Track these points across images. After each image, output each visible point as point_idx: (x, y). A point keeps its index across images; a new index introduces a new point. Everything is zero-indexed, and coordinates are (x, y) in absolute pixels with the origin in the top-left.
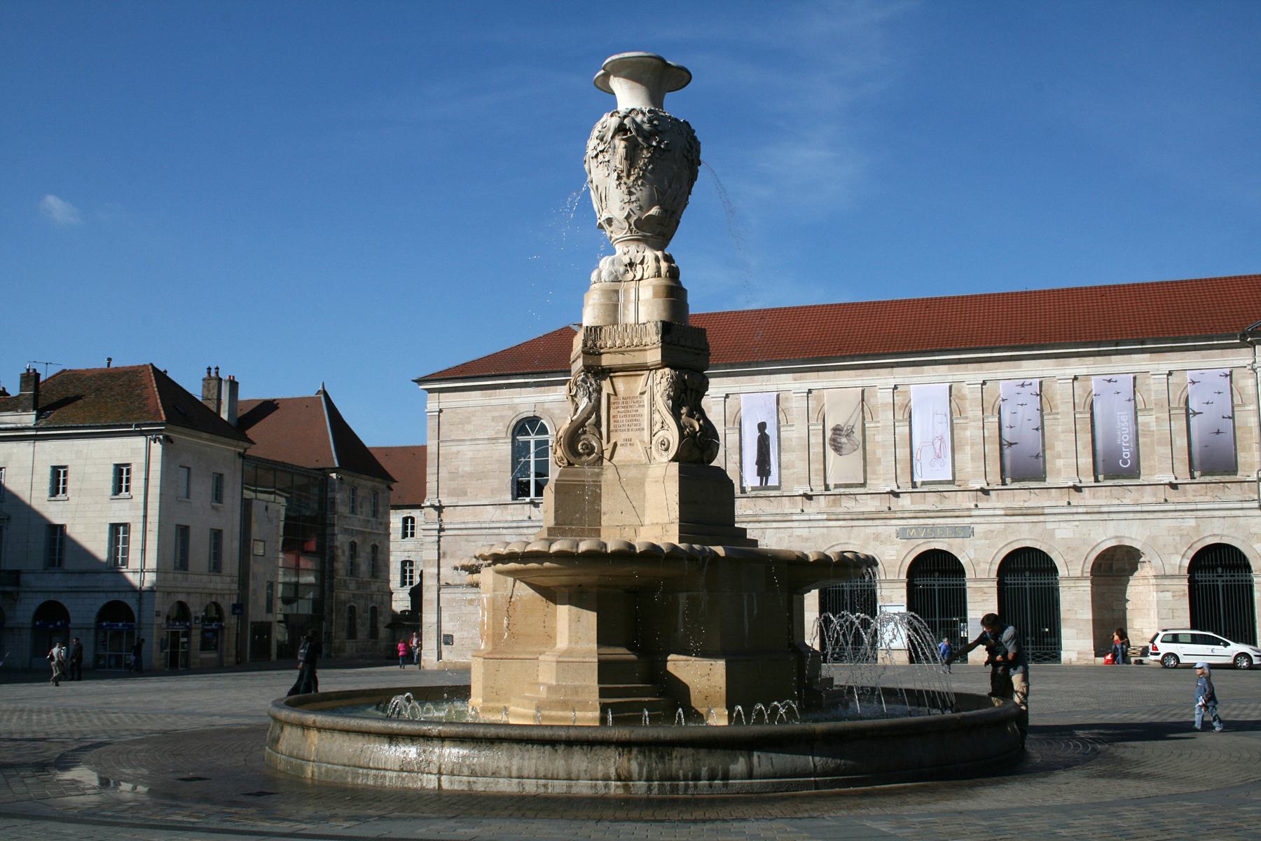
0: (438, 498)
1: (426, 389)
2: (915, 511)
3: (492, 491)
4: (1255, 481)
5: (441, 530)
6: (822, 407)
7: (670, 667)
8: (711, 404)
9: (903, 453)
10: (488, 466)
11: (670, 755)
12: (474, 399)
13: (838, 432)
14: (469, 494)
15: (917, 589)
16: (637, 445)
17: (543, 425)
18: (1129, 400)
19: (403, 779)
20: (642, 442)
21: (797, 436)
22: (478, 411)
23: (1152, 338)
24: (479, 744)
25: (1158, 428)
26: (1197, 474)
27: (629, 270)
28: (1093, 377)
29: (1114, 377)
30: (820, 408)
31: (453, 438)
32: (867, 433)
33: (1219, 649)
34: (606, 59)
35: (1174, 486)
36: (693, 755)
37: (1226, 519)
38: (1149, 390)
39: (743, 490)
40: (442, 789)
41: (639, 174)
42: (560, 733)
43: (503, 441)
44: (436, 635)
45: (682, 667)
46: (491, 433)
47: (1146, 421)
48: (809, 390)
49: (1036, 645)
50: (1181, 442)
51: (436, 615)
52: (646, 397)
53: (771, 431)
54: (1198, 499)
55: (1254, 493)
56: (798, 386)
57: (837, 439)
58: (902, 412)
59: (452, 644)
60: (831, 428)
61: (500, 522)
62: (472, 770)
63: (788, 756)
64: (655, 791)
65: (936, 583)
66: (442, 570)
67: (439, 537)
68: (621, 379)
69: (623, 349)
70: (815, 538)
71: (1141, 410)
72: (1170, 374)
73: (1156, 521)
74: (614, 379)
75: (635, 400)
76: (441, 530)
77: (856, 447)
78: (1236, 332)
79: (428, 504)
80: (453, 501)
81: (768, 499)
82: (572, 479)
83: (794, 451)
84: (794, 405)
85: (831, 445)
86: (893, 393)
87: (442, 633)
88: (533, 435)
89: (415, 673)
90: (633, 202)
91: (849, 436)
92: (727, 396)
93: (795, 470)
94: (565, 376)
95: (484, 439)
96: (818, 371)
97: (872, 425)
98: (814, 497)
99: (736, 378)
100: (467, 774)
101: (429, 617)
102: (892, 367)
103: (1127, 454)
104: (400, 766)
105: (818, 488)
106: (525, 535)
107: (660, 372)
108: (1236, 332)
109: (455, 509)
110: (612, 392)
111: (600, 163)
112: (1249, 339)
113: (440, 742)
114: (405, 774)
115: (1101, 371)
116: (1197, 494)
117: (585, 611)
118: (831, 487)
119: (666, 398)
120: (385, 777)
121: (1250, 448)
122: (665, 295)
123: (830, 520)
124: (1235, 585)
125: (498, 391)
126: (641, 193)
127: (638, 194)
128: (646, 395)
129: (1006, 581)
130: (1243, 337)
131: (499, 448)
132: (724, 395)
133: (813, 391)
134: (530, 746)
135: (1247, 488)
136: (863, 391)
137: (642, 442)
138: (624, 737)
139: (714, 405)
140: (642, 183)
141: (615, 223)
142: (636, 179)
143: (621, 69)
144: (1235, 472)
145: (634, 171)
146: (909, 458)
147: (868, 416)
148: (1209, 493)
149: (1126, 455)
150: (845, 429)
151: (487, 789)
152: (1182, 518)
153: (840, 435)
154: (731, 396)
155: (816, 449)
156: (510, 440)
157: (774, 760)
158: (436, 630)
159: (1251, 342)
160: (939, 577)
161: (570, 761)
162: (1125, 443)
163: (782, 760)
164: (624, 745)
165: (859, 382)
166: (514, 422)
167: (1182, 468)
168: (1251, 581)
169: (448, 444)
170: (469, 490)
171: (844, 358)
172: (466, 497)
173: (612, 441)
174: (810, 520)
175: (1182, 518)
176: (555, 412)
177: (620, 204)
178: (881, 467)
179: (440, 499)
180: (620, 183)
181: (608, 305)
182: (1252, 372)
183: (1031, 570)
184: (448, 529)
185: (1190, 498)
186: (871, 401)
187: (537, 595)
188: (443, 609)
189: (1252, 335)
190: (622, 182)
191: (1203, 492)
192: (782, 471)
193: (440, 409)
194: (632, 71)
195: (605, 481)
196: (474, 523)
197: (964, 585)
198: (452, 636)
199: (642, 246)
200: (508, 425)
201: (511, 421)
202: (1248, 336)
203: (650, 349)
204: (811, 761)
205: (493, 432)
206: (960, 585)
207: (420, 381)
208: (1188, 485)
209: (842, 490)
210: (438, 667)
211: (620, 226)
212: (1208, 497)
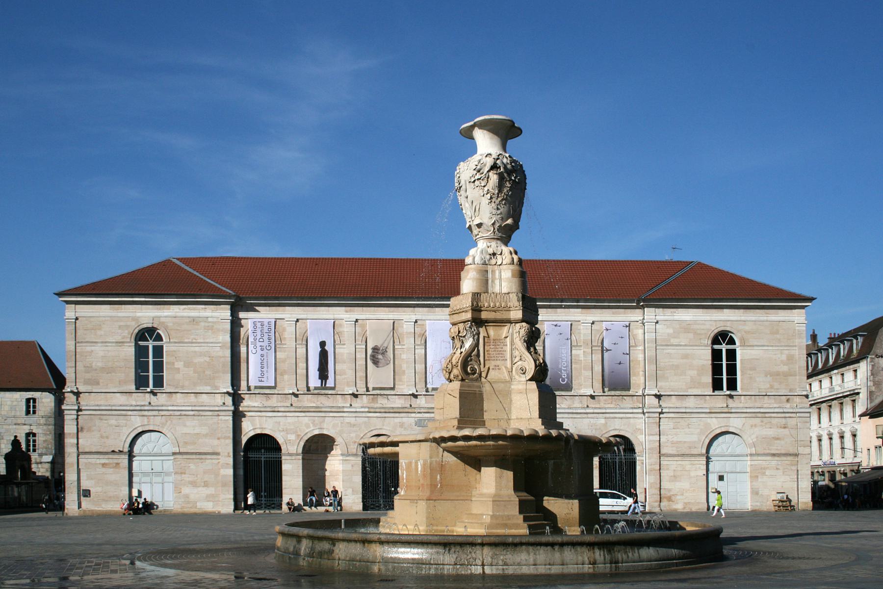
0: (76, 385)
1: (65, 301)
2: (428, 408)
3: (120, 382)
4: (641, 396)
5: (79, 410)
6: (365, 332)
7: (545, 504)
8: (286, 326)
9: (420, 367)
10: (116, 363)
11: (613, 549)
12: (105, 311)
13: (376, 351)
14: (101, 384)
15: (250, 460)
16: (503, 369)
17: (159, 334)
18: (568, 339)
19: (457, 569)
20: (506, 367)
21: (348, 352)
22: (108, 320)
23: (584, 299)
24: (508, 547)
25: (585, 359)
26: (606, 389)
27: (492, 258)
28: (545, 322)
29: (559, 323)
30: (364, 333)
31: (87, 340)
32: (396, 352)
33: (620, 501)
34: (476, 118)
35: (592, 397)
36: (624, 549)
37: (623, 419)
38: (580, 333)
39: (249, 388)
40: (485, 574)
41: (504, 197)
42: (558, 539)
43: (128, 344)
44: (77, 490)
45: (552, 504)
46: (119, 339)
47: (578, 354)
48: (356, 319)
49: (386, 499)
50: (598, 368)
51: (77, 475)
52: (508, 340)
53: (329, 348)
54: (607, 406)
55: (640, 403)
56: (348, 316)
57: (377, 356)
58: (420, 339)
59: (90, 497)
60: (371, 347)
61: (127, 406)
62: (505, 562)
63: (664, 549)
64: (614, 570)
65: (263, 456)
66: (80, 441)
67: (78, 416)
68: (492, 327)
69: (495, 309)
70: (359, 424)
71: (574, 346)
72: (593, 323)
73: (581, 419)
74: (487, 327)
75: (501, 341)
76: (79, 410)
77: (389, 362)
78: (634, 298)
79: (69, 390)
80: (88, 388)
81: (327, 396)
82: (466, 389)
83: (345, 363)
84: (345, 330)
85: (371, 359)
86: (415, 325)
87: (82, 488)
88: (151, 342)
89: (60, 518)
90: (498, 215)
91: (384, 354)
92: (297, 321)
93: (346, 376)
94: (177, 298)
95: (113, 342)
96: (363, 307)
97: (400, 347)
98: (359, 396)
99: (304, 308)
100: (501, 564)
101: (70, 477)
102: (414, 307)
103: (564, 375)
104: (455, 562)
105: (362, 390)
106: (147, 416)
107: (518, 325)
108: (634, 298)
109: (90, 395)
110: (486, 335)
111: (477, 187)
112: (642, 304)
113: (443, 547)
114: (458, 566)
115: (551, 318)
116: (606, 403)
117: (505, 471)
118: (370, 389)
119: (523, 342)
120: (444, 568)
121: (639, 374)
122: (519, 276)
123: (370, 412)
124: (630, 461)
125: (123, 306)
126: (503, 209)
127: (502, 210)
128: (508, 338)
129: (249, 456)
130: (638, 302)
131: (125, 349)
132: (296, 320)
133: (359, 321)
134: (539, 547)
135: (636, 400)
136: (394, 323)
137: (506, 367)
138: (592, 541)
139: (288, 326)
140: (505, 203)
141: (484, 226)
142: (502, 200)
143: (482, 125)
144: (629, 389)
145: (501, 195)
146: (424, 371)
147: (397, 341)
148: (614, 403)
149: (565, 376)
150: (381, 349)
151: (515, 573)
152: (597, 418)
153: (377, 353)
154: (300, 321)
155: (361, 362)
156: (134, 344)
157: (659, 552)
158: (77, 486)
159: (642, 305)
160: (264, 452)
161: (563, 555)
162: (564, 367)
163: (663, 551)
164: (591, 545)
165: (391, 316)
166: (136, 331)
167: (598, 385)
168: (635, 459)
169: (84, 344)
170: (101, 381)
171: (381, 299)
172: (99, 386)
173: (487, 367)
174: (356, 412)
175: (597, 418)
176: (168, 325)
177: (489, 215)
178: (405, 377)
179: (77, 386)
180: (491, 201)
181: (480, 279)
182: (642, 325)
183: (265, 449)
184: (84, 410)
185: (602, 405)
186: (399, 330)
187: (459, 461)
188: (81, 470)
189: (644, 301)
190: (493, 201)
191: (610, 401)
192: (337, 377)
193: (76, 317)
194: (492, 127)
195: (485, 391)
196: (106, 406)
197: (281, 458)
198: (89, 491)
199: (499, 242)
200: (132, 332)
201: (134, 330)
202: (641, 301)
203: (513, 310)
204: (674, 552)
205: (120, 337)
206: (278, 458)
207: (60, 294)
208: (601, 397)
209: (378, 392)
210: (79, 514)
211: (487, 229)
212: (612, 405)
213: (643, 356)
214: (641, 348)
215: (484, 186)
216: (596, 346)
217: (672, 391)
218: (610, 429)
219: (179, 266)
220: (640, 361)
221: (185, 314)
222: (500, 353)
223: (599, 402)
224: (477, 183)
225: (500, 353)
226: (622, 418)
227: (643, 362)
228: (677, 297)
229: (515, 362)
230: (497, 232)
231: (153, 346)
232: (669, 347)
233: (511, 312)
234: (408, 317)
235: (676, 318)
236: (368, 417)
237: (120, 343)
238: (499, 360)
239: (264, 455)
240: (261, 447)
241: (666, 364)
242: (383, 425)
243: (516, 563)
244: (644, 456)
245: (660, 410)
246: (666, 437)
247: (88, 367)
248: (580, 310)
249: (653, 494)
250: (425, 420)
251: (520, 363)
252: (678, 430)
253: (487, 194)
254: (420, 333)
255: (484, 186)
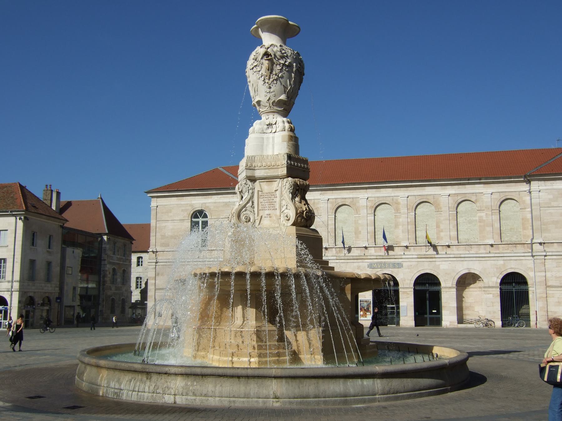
5: (156, 263)
12: (173, 201)
17: (205, 214)
31: (163, 219)
46: (181, 218)
52: (278, 193)
66: (157, 281)
79: (151, 250)
88: (201, 219)
94: (216, 191)
102: (366, 189)
107: (285, 180)
109: (163, 253)
111: (255, 72)
119: (288, 193)
131: (185, 224)
135: (526, 247)
148: (509, 249)
156: (190, 221)
160: (428, 286)
166: (192, 212)
173: (260, 216)
182: (529, 193)
183: (428, 283)
194: (272, 27)
200: (189, 213)
213: (530, 215)
214: (530, 209)
215: (259, 71)
216: (495, 210)
217: (554, 240)
218: (508, 268)
219: (222, 172)
220: (528, 219)
221: (221, 201)
222: (272, 203)
223: (498, 249)
224: (255, 69)
225: (272, 203)
226: (516, 260)
227: (531, 219)
228: (554, 172)
229: (283, 210)
230: (272, 106)
231: (202, 221)
232: (550, 208)
233: (540, 202)
234: (362, 195)
235: (555, 187)
236: (336, 263)
237: (182, 220)
238: (270, 210)
239: (515, 287)
240: (426, 282)
241: (548, 220)
242: (346, 268)
243: (203, 395)
244: (535, 287)
245: (545, 254)
246: (551, 273)
247: (163, 236)
248: (483, 185)
249: (542, 316)
250: (374, 264)
251: (286, 211)
252: (560, 268)
253: (261, 77)
254: (371, 206)
255: (259, 71)
